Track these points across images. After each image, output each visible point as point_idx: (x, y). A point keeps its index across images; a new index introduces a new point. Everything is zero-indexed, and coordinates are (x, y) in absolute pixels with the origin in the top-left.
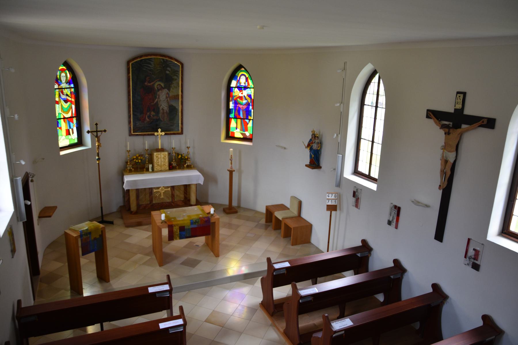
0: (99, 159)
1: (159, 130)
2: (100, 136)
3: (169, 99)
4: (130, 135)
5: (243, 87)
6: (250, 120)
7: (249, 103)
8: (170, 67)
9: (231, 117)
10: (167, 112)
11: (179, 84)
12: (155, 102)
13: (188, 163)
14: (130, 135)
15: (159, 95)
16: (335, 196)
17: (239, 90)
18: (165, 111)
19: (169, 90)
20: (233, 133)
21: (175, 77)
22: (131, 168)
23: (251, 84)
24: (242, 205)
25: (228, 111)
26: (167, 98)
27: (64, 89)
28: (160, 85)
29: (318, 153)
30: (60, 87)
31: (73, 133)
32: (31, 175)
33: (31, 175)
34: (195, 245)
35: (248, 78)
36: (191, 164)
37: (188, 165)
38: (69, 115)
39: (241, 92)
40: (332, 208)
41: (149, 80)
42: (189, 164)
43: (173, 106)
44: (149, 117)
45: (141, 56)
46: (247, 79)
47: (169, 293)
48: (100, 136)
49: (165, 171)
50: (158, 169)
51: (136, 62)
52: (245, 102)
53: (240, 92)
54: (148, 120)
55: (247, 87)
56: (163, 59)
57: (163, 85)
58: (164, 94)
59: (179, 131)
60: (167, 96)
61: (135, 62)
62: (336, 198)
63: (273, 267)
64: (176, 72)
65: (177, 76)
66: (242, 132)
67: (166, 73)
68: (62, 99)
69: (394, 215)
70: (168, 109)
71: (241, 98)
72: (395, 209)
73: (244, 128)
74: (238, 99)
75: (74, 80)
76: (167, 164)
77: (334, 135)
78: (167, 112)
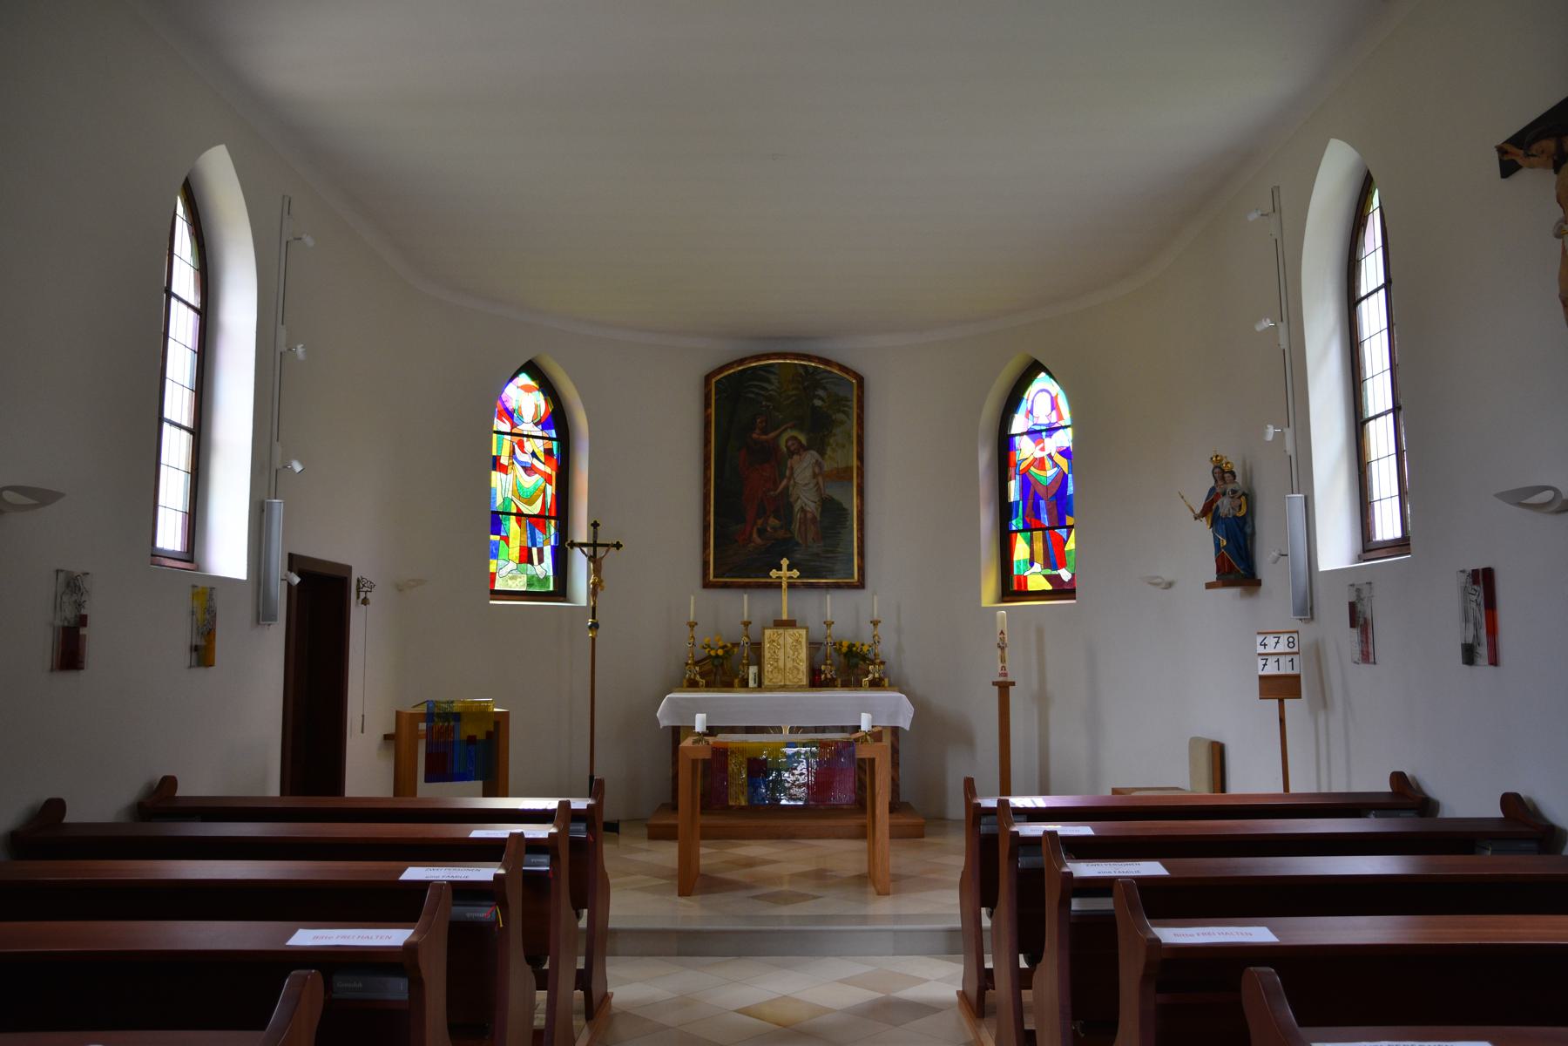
0: (595, 626)
1: (782, 562)
2: (602, 558)
3: (820, 479)
4: (707, 585)
5: (1044, 428)
6: (1070, 528)
7: (1064, 473)
8: (825, 389)
10: (814, 518)
11: (850, 436)
12: (779, 490)
13: (874, 672)
14: (707, 585)
15: (792, 468)
16: (1290, 643)
17: (1034, 441)
18: (809, 515)
19: (822, 453)
20: (1023, 580)
21: (841, 416)
25: (1005, 511)
26: (815, 476)
27: (525, 439)
28: (795, 438)
29: (1242, 530)
30: (515, 431)
31: (541, 560)
32: (364, 585)
33: (364, 585)
36: (882, 675)
38: (535, 509)
39: (1041, 445)
40: (1280, 688)
41: (764, 424)
42: (877, 675)
44: (761, 532)
45: (741, 361)
46: (1054, 405)
47: (588, 828)
48: (602, 558)
49: (800, 688)
50: (774, 680)
51: (729, 375)
52: (1051, 472)
53: (1036, 446)
55: (1057, 425)
57: (803, 439)
59: (853, 578)
60: (817, 470)
61: (725, 377)
62: (1295, 649)
64: (844, 402)
66: (1048, 572)
67: (813, 405)
68: (519, 462)
69: (1478, 615)
70: (820, 509)
71: (1040, 463)
72: (1476, 587)
73: (1054, 558)
74: (1032, 468)
75: (557, 420)
76: (803, 666)
77: (1267, 428)
78: (814, 518)
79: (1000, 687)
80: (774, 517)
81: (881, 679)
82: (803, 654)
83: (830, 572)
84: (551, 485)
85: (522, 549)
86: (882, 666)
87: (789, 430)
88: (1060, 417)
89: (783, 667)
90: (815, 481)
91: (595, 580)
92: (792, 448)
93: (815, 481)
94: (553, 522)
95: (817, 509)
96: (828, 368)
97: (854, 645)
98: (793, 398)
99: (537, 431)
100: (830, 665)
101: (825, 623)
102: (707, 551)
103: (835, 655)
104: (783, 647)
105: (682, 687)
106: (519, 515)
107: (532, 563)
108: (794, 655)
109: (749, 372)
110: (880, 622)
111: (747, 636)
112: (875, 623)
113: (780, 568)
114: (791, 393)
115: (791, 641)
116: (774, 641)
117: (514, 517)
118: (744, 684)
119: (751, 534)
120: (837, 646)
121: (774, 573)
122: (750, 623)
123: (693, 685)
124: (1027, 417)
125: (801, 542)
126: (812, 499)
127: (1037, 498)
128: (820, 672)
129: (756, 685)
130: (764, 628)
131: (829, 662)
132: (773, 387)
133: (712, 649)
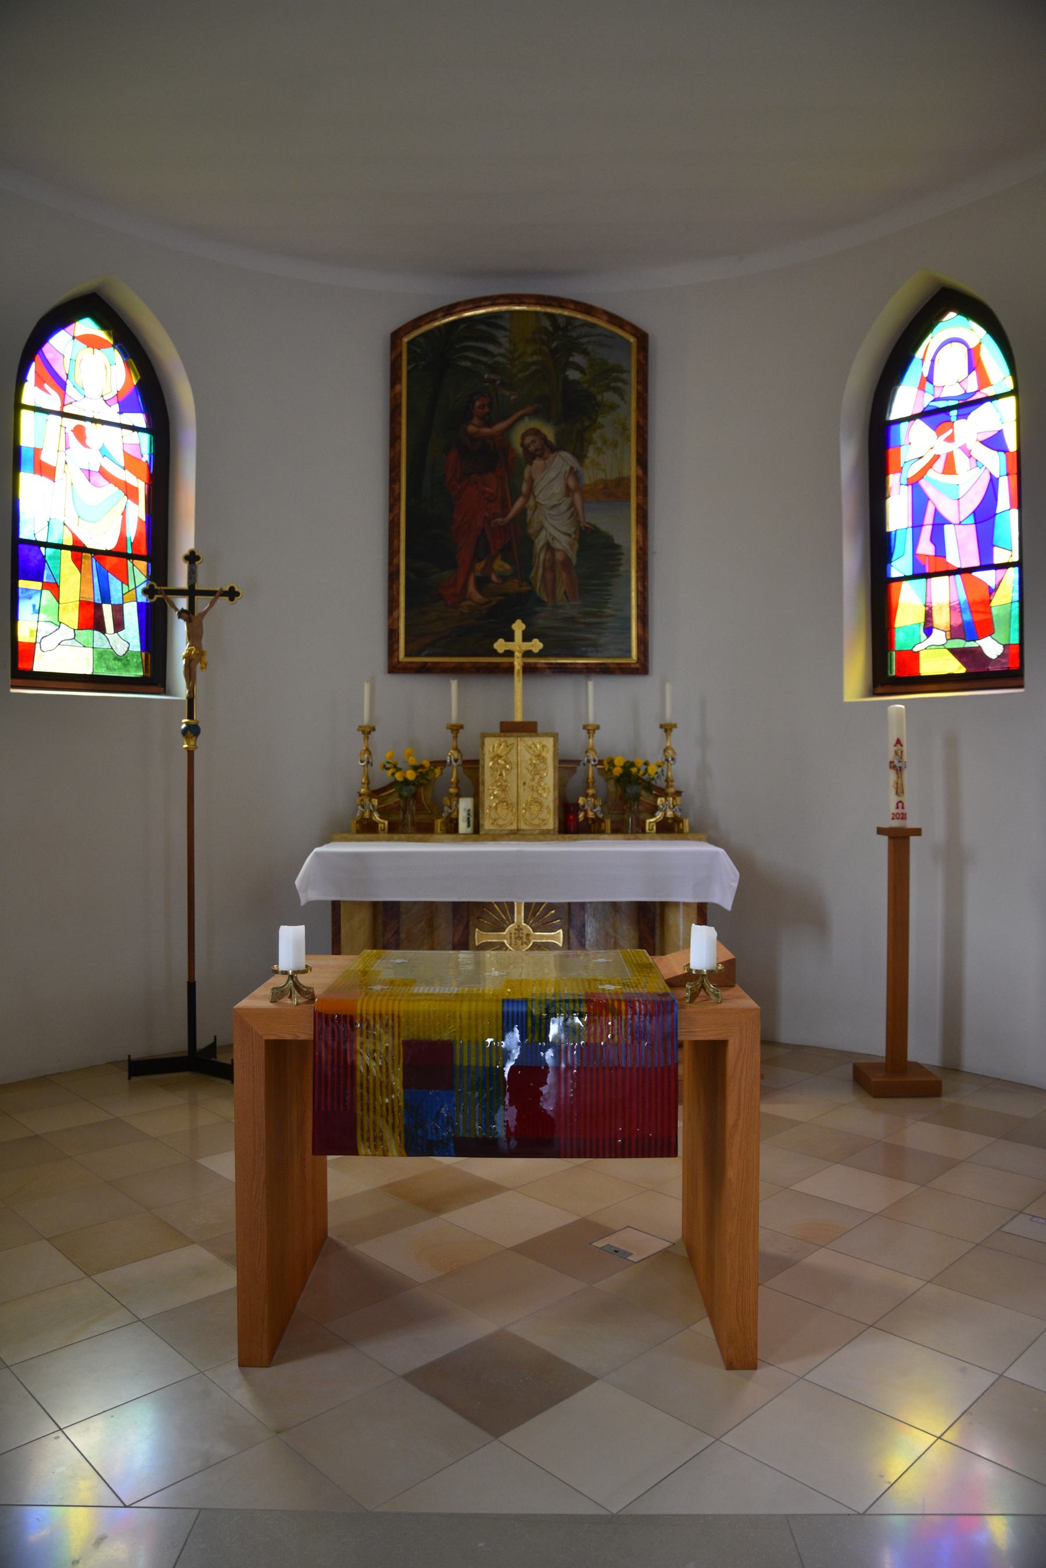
0: (192, 731)
3: (577, 497)
4: (394, 668)
8: (585, 352)
9: (894, 573)
11: (625, 429)
13: (664, 805)
14: (394, 668)
15: (532, 481)
17: (936, 428)
18: (559, 556)
19: (580, 456)
20: (913, 657)
21: (610, 397)
22: (376, 817)
23: (1000, 377)
24: (973, 1059)
26: (568, 492)
28: (536, 432)
30: (66, 410)
31: (119, 625)
34: (600, 1244)
35: (978, 347)
36: (679, 814)
37: (665, 818)
41: (487, 410)
42: (670, 814)
43: (595, 531)
44: (482, 583)
46: (974, 363)
49: (542, 835)
50: (500, 822)
54: (477, 597)
56: (551, 317)
57: (549, 432)
58: (552, 474)
59: (630, 656)
60: (572, 483)
63: (148, 422)
64: (614, 374)
65: (617, 390)
67: (566, 377)
70: (576, 546)
76: (549, 798)
79: (890, 838)
80: (502, 559)
81: (677, 820)
82: (549, 777)
83: (595, 648)
84: (136, 501)
85: (83, 604)
86: (678, 799)
87: (526, 419)
88: (984, 381)
89: (514, 800)
90: (568, 501)
91: (190, 651)
92: (532, 448)
93: (568, 501)
94: (143, 565)
95: (571, 545)
96: (590, 319)
97: (633, 765)
98: (533, 368)
99: (112, 413)
100: (593, 796)
101: (584, 727)
102: (395, 614)
103: (600, 780)
104: (515, 766)
105: (349, 831)
106: (78, 549)
107: (102, 629)
108: (533, 779)
109: (462, 326)
110: (675, 726)
111: (456, 749)
112: (667, 729)
113: (510, 637)
114: (530, 360)
115: (528, 756)
116: (500, 757)
117: (69, 553)
118: (451, 828)
119: (465, 586)
120: (605, 766)
121: (500, 645)
122: (462, 727)
123: (367, 829)
124: (921, 388)
125: (546, 600)
126: (565, 529)
127: (939, 524)
128: (577, 808)
129: (470, 830)
130: (484, 736)
131: (591, 791)
132: (502, 351)
133: (398, 770)
